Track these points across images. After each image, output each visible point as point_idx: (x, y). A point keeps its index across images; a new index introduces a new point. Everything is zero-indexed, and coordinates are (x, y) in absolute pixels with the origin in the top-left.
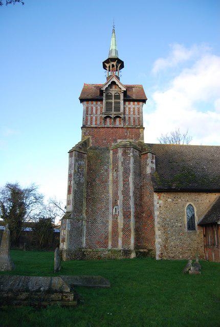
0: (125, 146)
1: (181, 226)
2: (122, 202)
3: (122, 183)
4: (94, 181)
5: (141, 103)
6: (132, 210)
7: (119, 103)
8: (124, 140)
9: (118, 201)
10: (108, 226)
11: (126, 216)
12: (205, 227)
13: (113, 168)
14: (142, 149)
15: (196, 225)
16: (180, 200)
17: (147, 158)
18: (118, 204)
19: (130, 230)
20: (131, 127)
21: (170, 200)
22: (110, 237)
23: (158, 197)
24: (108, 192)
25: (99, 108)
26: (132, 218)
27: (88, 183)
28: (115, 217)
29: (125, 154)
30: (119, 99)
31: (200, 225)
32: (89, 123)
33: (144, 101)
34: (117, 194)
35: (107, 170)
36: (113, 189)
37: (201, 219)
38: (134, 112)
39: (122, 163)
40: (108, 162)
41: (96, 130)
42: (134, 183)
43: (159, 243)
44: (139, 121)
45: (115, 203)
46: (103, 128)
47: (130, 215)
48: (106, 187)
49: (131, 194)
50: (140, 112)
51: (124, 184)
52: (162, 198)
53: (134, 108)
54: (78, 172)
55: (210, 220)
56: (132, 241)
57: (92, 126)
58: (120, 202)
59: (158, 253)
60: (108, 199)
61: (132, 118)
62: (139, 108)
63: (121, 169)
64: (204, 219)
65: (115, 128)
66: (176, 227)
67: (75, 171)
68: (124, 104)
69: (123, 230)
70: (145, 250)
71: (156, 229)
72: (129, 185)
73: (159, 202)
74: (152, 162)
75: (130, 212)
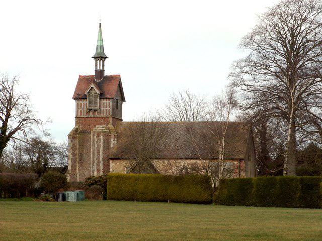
29: (98, 136)
40: (90, 141)
58: (95, 164)
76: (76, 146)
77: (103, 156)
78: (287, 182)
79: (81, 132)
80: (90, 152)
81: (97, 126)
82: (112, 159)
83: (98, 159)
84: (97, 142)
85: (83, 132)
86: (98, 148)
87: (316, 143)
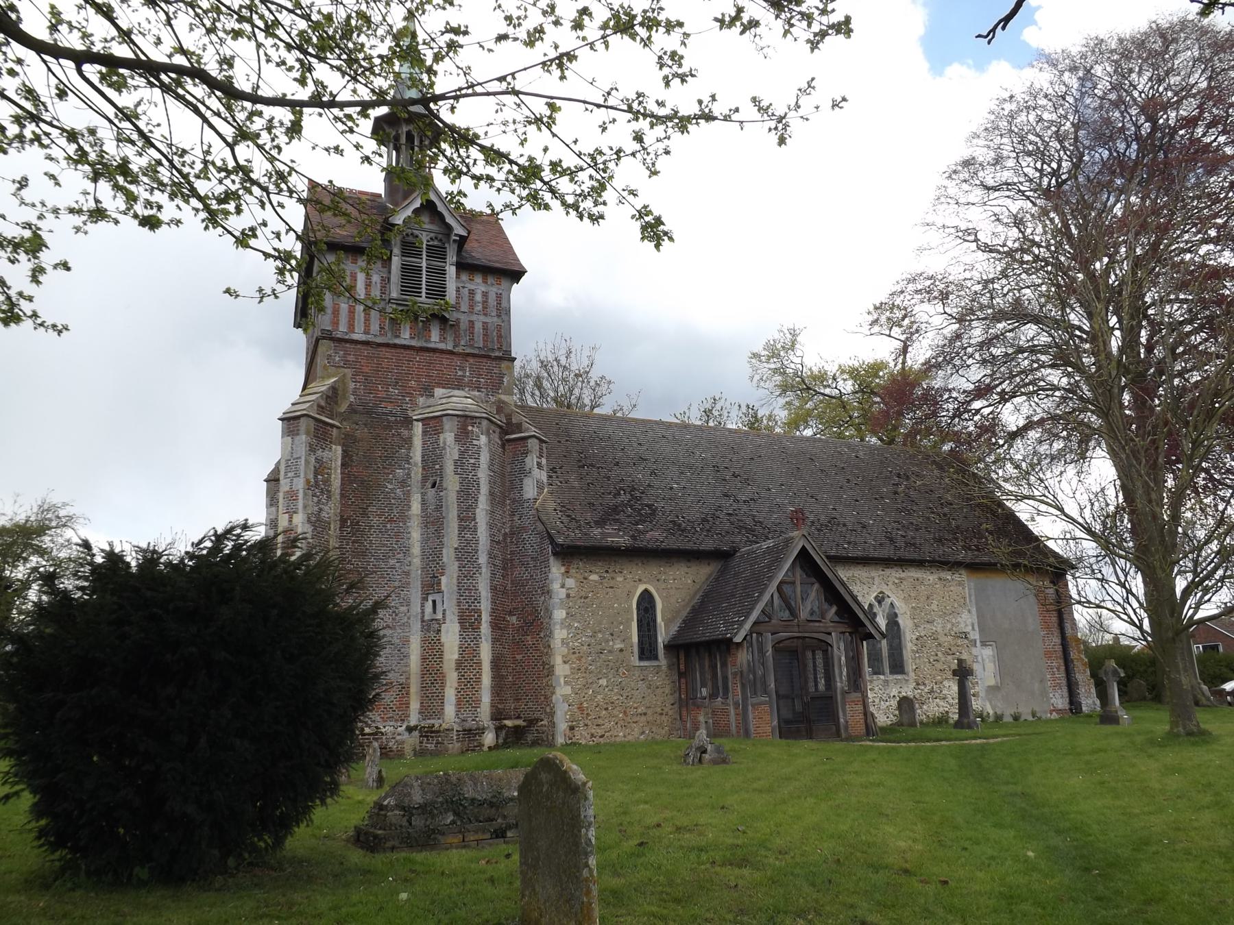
0: (465, 420)
1: (621, 650)
2: (455, 581)
3: (456, 525)
4: (365, 514)
5: (505, 283)
6: (485, 606)
7: (443, 272)
8: (456, 392)
9: (444, 580)
10: (407, 656)
11: (469, 622)
12: (687, 656)
13: (425, 479)
14: (509, 423)
15: (661, 646)
16: (620, 579)
17: (526, 453)
18: (443, 587)
19: (479, 664)
20: (476, 351)
21: (594, 577)
22: (414, 688)
23: (563, 569)
24: (407, 551)
25: (376, 278)
26: (485, 628)
27: (343, 521)
28: (432, 628)
29: (463, 436)
30: (443, 258)
31: (671, 647)
32: (343, 328)
33: (516, 274)
34: (439, 555)
35: (404, 483)
36: (425, 540)
37: (674, 629)
38: (485, 302)
39: (455, 462)
40: (408, 459)
41: (366, 351)
42: (491, 526)
43: (566, 698)
44: (500, 336)
45: (431, 586)
46: (387, 345)
47: (479, 619)
48: (400, 535)
49: (483, 559)
50: (504, 312)
51: (462, 529)
52: (573, 571)
53: (485, 294)
54: (317, 484)
55: (703, 633)
56: (486, 698)
57: (355, 337)
58: (448, 582)
59: (562, 726)
60: (407, 574)
61: (478, 327)
62: (499, 296)
63: (452, 483)
64: (681, 630)
65: (395, 346)
66: (610, 651)
67: (308, 482)
68: (458, 276)
69: (459, 665)
70: (520, 722)
71: (558, 660)
72: (475, 530)
73: (561, 582)
74: (539, 465)
75: (479, 612)
76: (327, 482)
77: (493, 541)
78: (970, 434)
79: (352, 410)
80: (404, 517)
81: (439, 392)
82: (569, 553)
83: (466, 554)
84: (459, 464)
85: (366, 412)
86: (467, 494)
87: (1113, 329)
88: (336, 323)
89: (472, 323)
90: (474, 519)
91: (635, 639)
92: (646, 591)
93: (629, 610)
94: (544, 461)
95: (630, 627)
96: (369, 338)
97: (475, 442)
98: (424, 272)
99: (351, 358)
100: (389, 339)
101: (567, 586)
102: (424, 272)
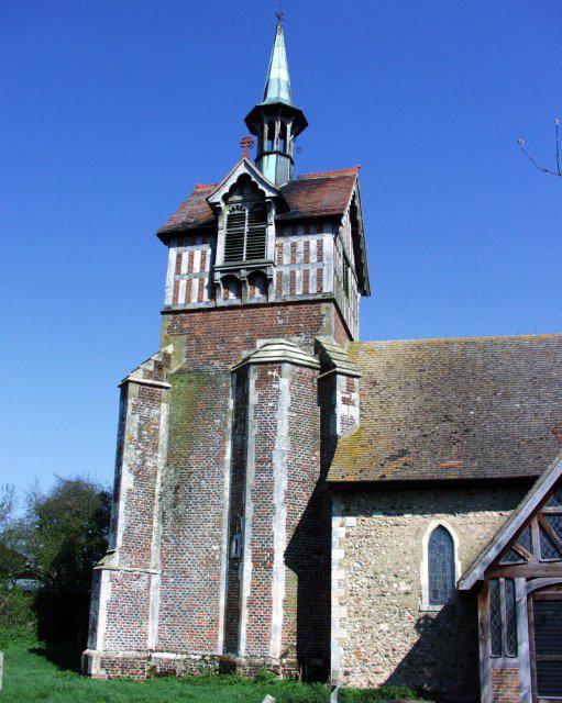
1: (407, 593)
7: (263, 232)
38: (307, 251)
41: (242, 314)
43: (341, 642)
51: (259, 470)
75: (271, 551)
81: (260, 343)
88: (175, 299)
89: (293, 273)
90: (271, 461)
91: (425, 581)
92: (441, 527)
93: (415, 551)
94: (355, 396)
95: (417, 563)
96: (202, 305)
97: (275, 386)
98: (246, 237)
99: (186, 326)
100: (212, 305)
101: (348, 524)
102: (246, 237)
